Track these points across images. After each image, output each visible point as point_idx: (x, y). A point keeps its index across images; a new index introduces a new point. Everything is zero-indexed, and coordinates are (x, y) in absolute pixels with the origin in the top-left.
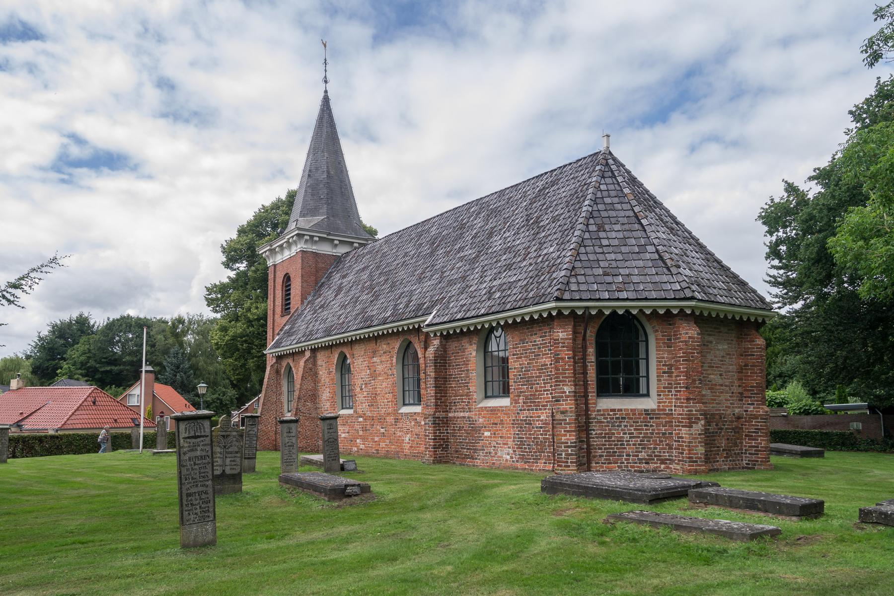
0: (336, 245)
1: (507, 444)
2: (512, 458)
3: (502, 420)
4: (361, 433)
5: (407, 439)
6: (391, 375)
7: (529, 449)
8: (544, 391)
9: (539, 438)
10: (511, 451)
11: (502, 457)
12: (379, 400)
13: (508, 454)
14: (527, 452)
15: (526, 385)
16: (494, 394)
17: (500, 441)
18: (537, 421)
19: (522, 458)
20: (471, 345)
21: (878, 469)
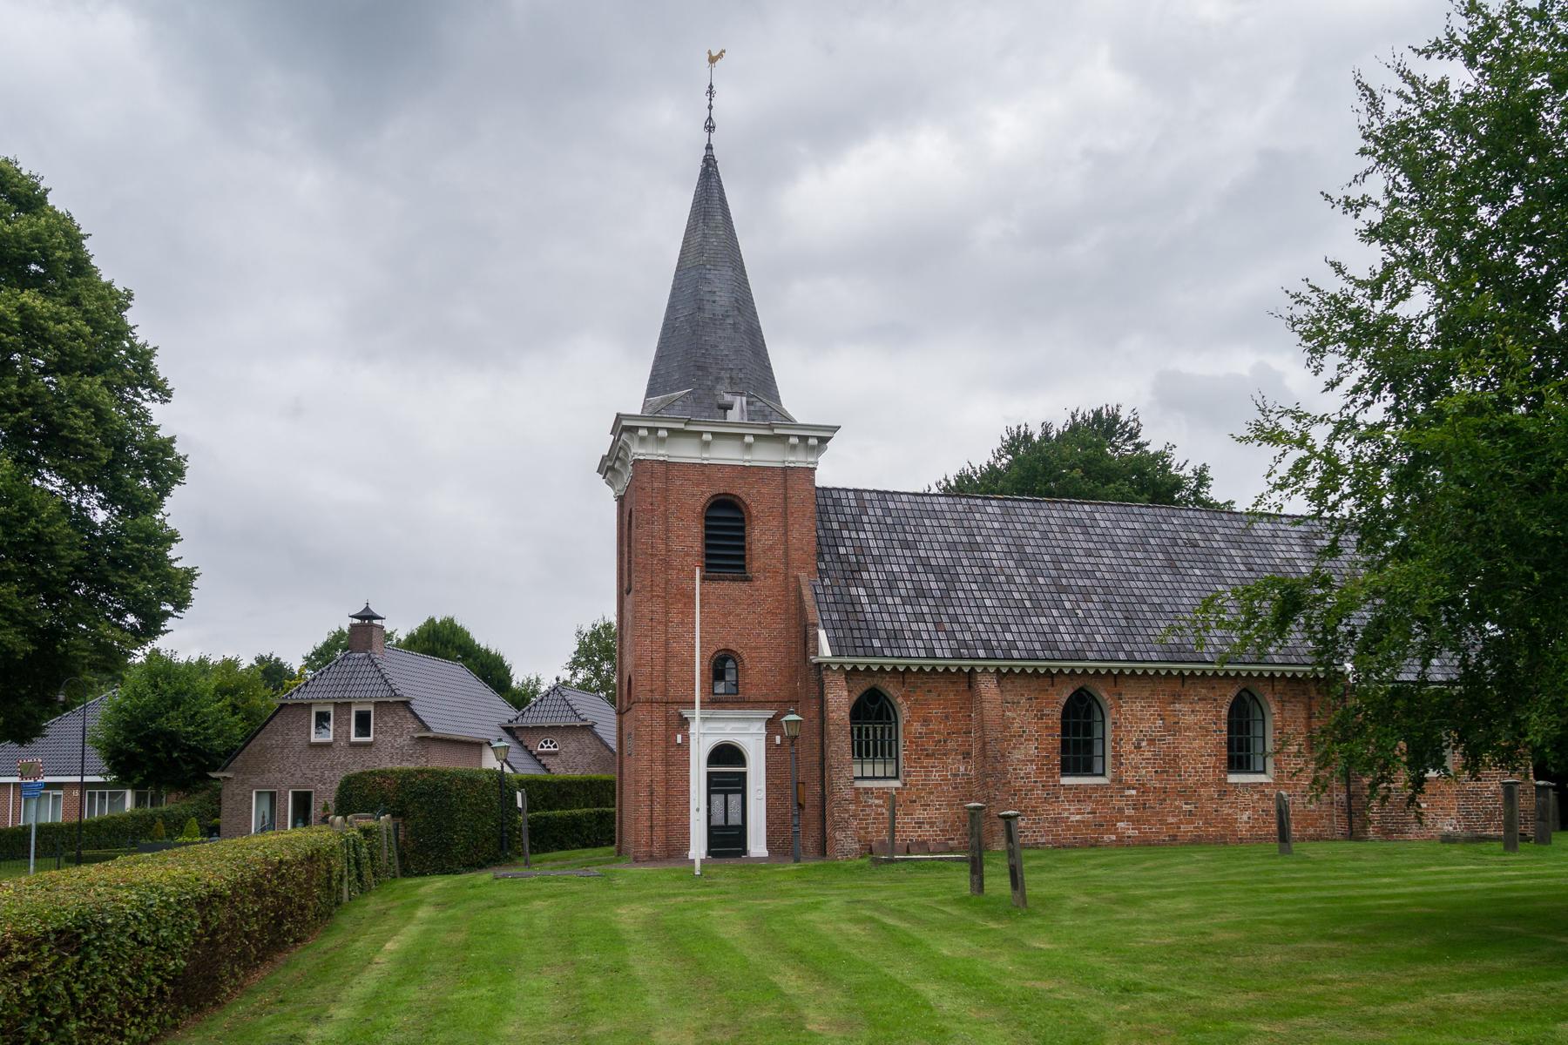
0: (707, 444)
1: (1449, 815)
2: (1455, 828)
4: (1129, 812)
5: (1245, 818)
6: (1215, 731)
10: (1454, 822)
12: (1185, 764)
16: (1257, 769)
17: (1440, 812)
21: (630, 900)
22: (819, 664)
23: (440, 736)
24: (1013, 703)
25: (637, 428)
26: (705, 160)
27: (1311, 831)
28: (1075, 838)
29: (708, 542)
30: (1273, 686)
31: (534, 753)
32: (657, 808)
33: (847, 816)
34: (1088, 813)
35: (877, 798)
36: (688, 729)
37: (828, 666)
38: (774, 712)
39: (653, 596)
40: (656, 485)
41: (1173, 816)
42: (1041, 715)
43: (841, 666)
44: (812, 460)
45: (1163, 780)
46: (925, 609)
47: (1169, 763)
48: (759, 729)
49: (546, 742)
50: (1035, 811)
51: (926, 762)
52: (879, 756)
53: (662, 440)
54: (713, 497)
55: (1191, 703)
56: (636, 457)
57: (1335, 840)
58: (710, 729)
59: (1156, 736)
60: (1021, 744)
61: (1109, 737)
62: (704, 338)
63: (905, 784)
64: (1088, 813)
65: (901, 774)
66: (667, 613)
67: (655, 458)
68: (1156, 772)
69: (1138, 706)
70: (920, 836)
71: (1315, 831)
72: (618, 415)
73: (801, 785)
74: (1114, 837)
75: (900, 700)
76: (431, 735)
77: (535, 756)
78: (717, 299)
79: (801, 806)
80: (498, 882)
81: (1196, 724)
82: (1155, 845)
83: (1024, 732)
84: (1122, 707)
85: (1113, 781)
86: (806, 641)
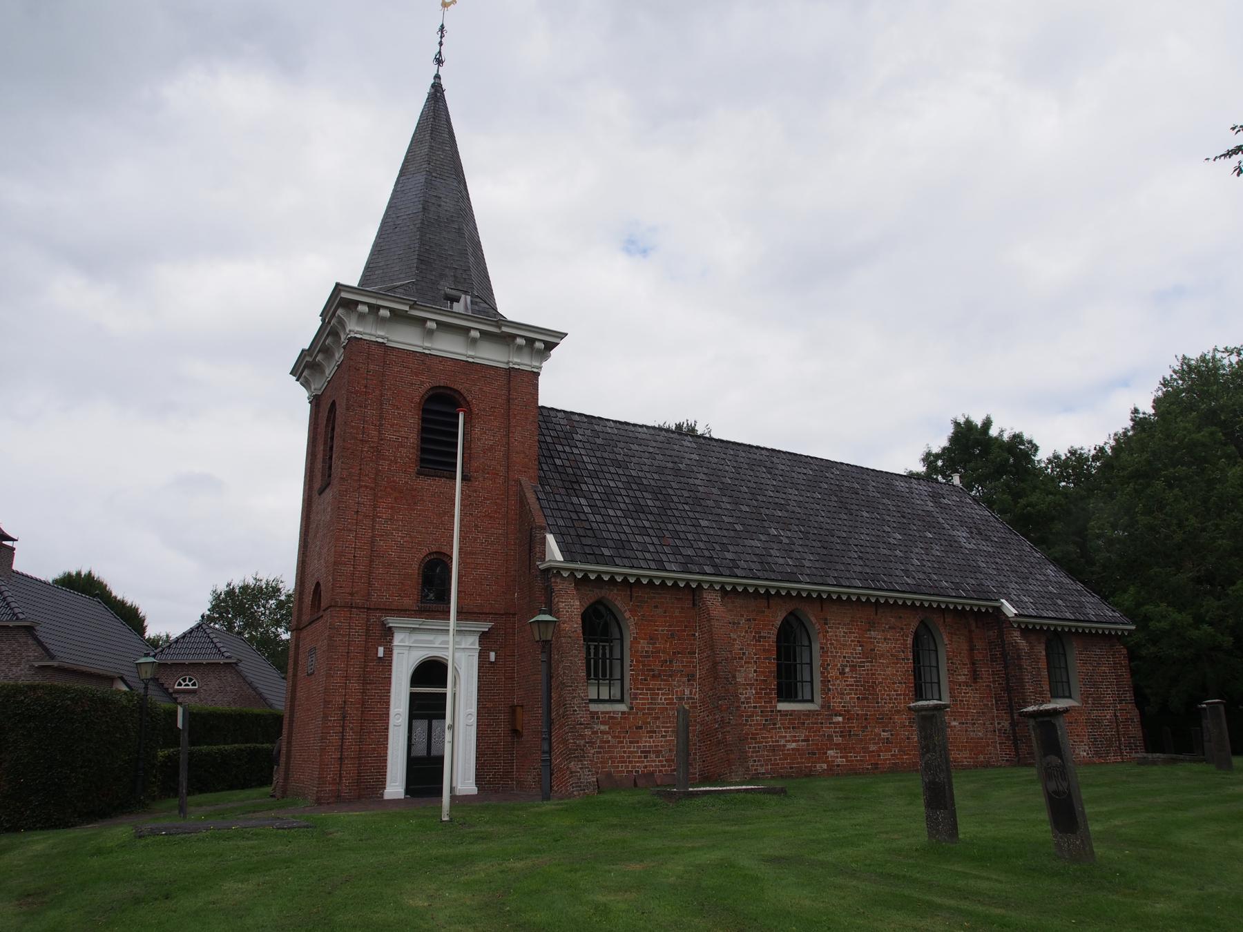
1: (1083, 742)
2: (1088, 754)
3: (1076, 719)
4: (837, 740)
6: (903, 659)
7: (1101, 744)
8: (1107, 694)
9: (1107, 735)
11: (1079, 754)
12: (880, 691)
13: (1085, 751)
14: (1099, 748)
15: (1092, 688)
16: (928, 698)
18: (1105, 719)
19: (1096, 753)
20: (1040, 643)
22: (548, 570)
23: (66, 666)
24: (734, 623)
25: (357, 303)
26: (433, 86)
27: (981, 758)
28: (791, 768)
29: (425, 435)
30: (944, 618)
31: (171, 690)
32: (349, 735)
33: (582, 742)
34: (803, 741)
35: (603, 723)
36: (391, 641)
37: (558, 572)
38: (490, 625)
39: (361, 487)
40: (371, 367)
41: (873, 743)
42: (760, 637)
43: (572, 572)
44: (537, 364)
45: (864, 706)
46: (647, 524)
47: (868, 690)
48: (472, 644)
49: (184, 680)
50: (756, 739)
51: (652, 684)
52: (592, 677)
53: (383, 320)
54: (432, 388)
55: (883, 631)
56: (352, 335)
57: (1000, 766)
58: (416, 641)
59: (857, 662)
60: (742, 667)
61: (817, 663)
62: (428, 235)
63: (631, 708)
64: (803, 741)
65: (626, 697)
66: (375, 507)
67: (373, 339)
68: (858, 698)
69: (841, 631)
70: (646, 767)
71: (985, 758)
72: (338, 285)
73: (519, 709)
74: (825, 766)
75: (627, 615)
76: (55, 664)
77: (171, 694)
78: (443, 204)
79: (516, 733)
80: (143, 842)
81: (888, 651)
82: (860, 774)
83: (744, 654)
84: (828, 632)
85: (822, 707)
86: (534, 547)
